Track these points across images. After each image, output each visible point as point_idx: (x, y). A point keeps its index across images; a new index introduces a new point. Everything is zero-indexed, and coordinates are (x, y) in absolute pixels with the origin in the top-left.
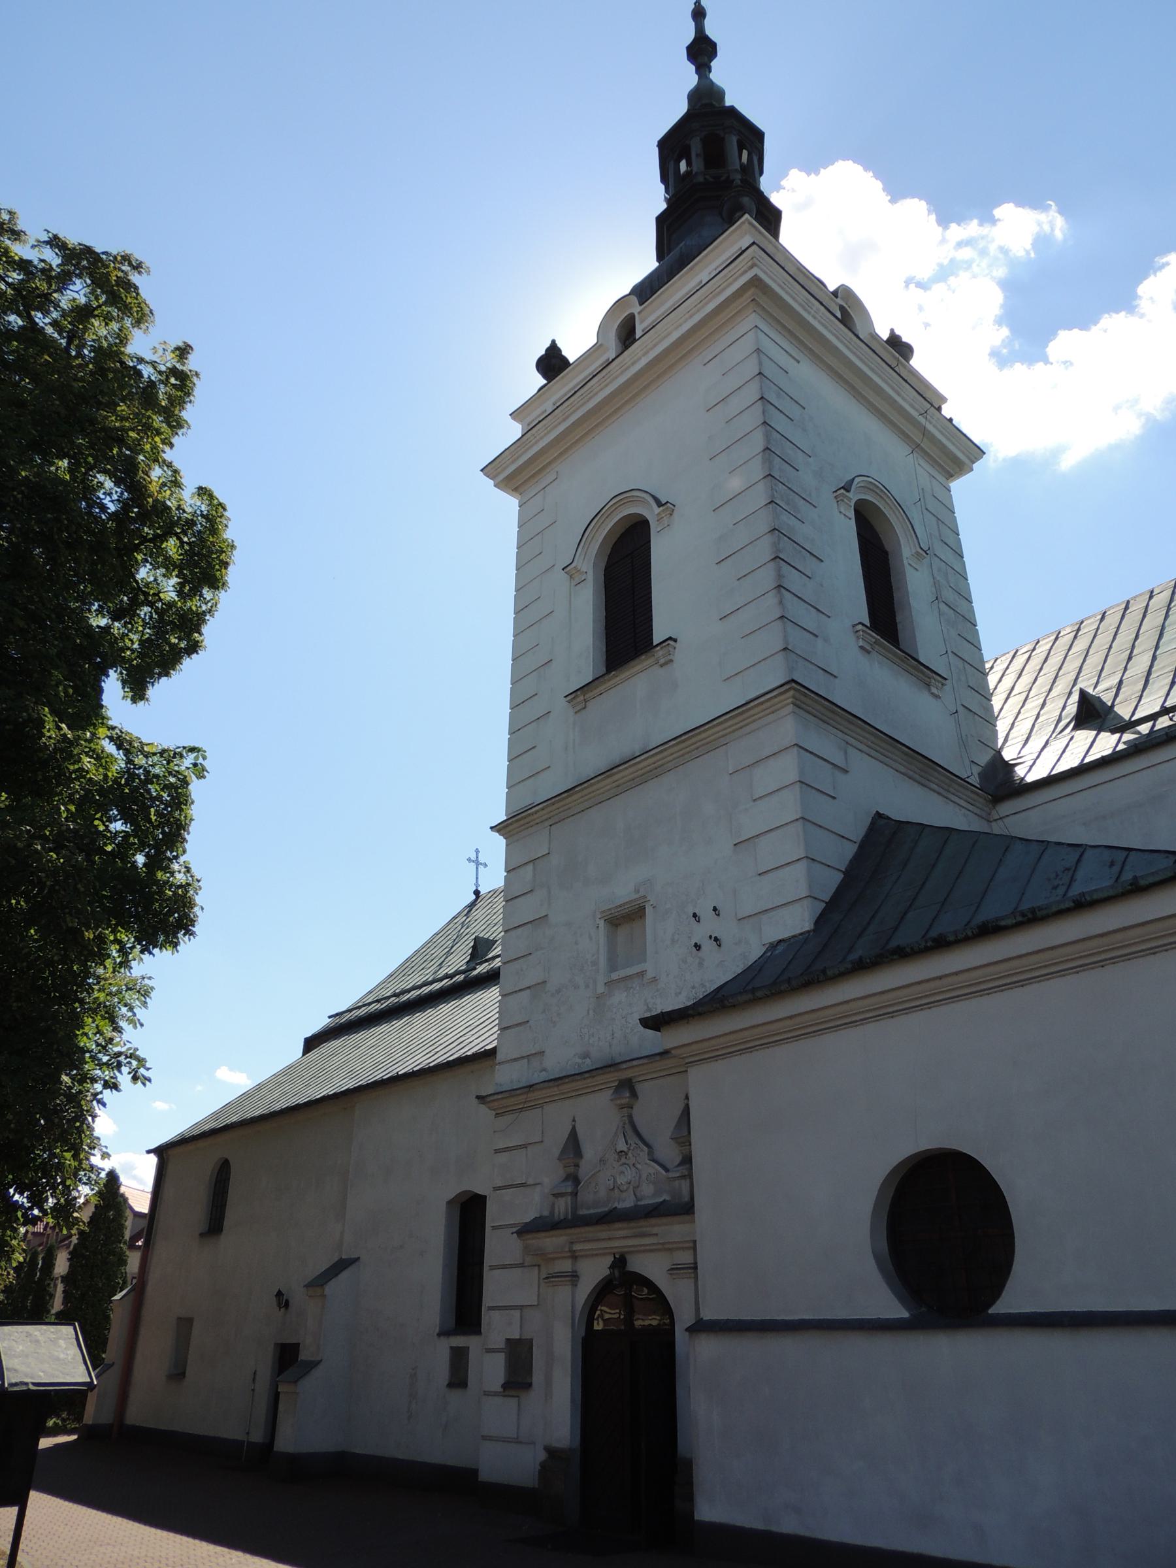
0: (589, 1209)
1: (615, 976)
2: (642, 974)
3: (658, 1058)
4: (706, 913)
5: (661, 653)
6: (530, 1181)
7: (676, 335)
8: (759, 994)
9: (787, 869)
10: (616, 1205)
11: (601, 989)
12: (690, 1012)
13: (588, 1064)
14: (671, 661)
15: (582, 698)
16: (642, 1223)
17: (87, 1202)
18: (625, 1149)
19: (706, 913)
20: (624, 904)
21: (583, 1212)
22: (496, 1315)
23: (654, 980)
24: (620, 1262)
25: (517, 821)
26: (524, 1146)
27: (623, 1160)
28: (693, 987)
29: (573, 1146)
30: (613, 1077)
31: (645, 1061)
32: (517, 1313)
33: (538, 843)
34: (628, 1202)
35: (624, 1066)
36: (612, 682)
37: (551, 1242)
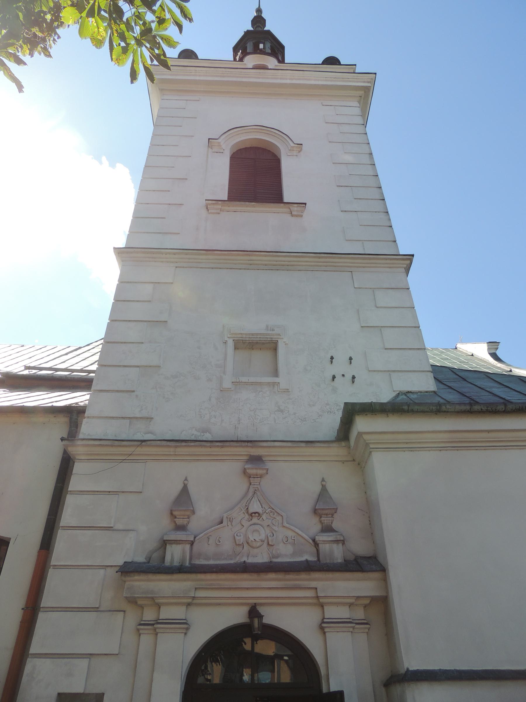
0: (208, 559)
1: (244, 379)
2: (274, 384)
3: (303, 445)
4: (341, 358)
5: (296, 209)
6: (119, 526)
7: (313, 82)
8: (476, 408)
9: (411, 352)
10: (245, 559)
11: (227, 384)
12: (406, 408)
13: (208, 436)
14: (302, 216)
15: (220, 207)
16: (303, 576)
17: (209, 680)
18: (260, 511)
19: (341, 358)
20: (257, 334)
21: (197, 562)
22: (38, 662)
23: (287, 391)
24: (254, 612)
25: (144, 253)
26: (116, 493)
27: (255, 520)
28: (327, 404)
29: (184, 497)
30: (245, 451)
31: (289, 444)
32: (83, 663)
33: (301, 213)
34: (261, 557)
35: (265, 444)
36: (249, 208)
37: (141, 584)
